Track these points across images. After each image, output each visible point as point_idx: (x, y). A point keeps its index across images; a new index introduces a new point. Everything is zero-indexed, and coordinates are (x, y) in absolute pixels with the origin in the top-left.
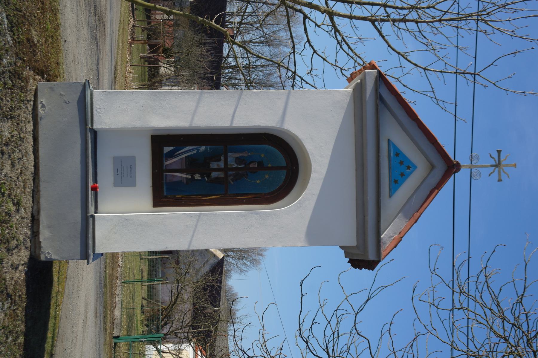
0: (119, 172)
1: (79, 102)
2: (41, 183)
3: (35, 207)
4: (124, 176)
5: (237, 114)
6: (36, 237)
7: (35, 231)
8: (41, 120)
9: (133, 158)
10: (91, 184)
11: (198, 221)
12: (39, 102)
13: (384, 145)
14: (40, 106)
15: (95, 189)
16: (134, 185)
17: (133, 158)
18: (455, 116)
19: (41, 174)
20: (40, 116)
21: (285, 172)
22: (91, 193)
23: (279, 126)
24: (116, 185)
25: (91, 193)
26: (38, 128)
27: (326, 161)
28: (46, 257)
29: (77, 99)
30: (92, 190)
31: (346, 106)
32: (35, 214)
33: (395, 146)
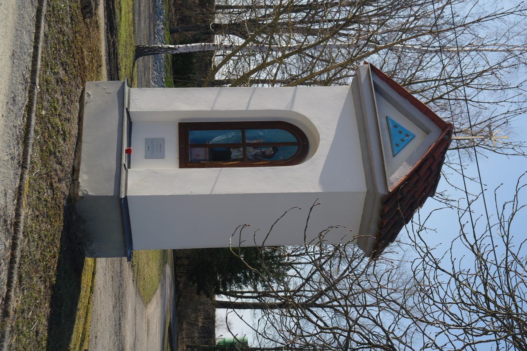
0: (150, 149)
1: (118, 93)
2: (83, 144)
3: (76, 161)
4: (154, 150)
5: (251, 102)
6: (76, 182)
7: (74, 178)
8: (86, 103)
9: (163, 139)
10: (125, 147)
11: (219, 173)
12: (86, 93)
13: (382, 122)
14: (86, 96)
15: (129, 151)
16: (163, 157)
17: (163, 139)
18: (466, 192)
19: (83, 138)
20: (85, 101)
21: (296, 147)
22: (124, 155)
23: (288, 109)
24: (146, 158)
25: (124, 155)
26: (83, 112)
27: (333, 133)
28: (83, 193)
29: (117, 91)
30: (126, 152)
31: (346, 96)
32: (76, 165)
33: (392, 121)
